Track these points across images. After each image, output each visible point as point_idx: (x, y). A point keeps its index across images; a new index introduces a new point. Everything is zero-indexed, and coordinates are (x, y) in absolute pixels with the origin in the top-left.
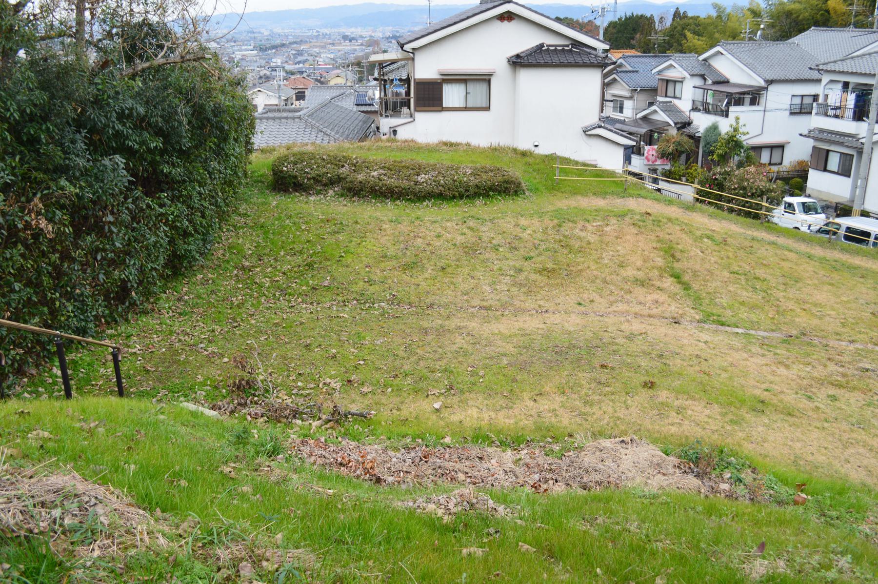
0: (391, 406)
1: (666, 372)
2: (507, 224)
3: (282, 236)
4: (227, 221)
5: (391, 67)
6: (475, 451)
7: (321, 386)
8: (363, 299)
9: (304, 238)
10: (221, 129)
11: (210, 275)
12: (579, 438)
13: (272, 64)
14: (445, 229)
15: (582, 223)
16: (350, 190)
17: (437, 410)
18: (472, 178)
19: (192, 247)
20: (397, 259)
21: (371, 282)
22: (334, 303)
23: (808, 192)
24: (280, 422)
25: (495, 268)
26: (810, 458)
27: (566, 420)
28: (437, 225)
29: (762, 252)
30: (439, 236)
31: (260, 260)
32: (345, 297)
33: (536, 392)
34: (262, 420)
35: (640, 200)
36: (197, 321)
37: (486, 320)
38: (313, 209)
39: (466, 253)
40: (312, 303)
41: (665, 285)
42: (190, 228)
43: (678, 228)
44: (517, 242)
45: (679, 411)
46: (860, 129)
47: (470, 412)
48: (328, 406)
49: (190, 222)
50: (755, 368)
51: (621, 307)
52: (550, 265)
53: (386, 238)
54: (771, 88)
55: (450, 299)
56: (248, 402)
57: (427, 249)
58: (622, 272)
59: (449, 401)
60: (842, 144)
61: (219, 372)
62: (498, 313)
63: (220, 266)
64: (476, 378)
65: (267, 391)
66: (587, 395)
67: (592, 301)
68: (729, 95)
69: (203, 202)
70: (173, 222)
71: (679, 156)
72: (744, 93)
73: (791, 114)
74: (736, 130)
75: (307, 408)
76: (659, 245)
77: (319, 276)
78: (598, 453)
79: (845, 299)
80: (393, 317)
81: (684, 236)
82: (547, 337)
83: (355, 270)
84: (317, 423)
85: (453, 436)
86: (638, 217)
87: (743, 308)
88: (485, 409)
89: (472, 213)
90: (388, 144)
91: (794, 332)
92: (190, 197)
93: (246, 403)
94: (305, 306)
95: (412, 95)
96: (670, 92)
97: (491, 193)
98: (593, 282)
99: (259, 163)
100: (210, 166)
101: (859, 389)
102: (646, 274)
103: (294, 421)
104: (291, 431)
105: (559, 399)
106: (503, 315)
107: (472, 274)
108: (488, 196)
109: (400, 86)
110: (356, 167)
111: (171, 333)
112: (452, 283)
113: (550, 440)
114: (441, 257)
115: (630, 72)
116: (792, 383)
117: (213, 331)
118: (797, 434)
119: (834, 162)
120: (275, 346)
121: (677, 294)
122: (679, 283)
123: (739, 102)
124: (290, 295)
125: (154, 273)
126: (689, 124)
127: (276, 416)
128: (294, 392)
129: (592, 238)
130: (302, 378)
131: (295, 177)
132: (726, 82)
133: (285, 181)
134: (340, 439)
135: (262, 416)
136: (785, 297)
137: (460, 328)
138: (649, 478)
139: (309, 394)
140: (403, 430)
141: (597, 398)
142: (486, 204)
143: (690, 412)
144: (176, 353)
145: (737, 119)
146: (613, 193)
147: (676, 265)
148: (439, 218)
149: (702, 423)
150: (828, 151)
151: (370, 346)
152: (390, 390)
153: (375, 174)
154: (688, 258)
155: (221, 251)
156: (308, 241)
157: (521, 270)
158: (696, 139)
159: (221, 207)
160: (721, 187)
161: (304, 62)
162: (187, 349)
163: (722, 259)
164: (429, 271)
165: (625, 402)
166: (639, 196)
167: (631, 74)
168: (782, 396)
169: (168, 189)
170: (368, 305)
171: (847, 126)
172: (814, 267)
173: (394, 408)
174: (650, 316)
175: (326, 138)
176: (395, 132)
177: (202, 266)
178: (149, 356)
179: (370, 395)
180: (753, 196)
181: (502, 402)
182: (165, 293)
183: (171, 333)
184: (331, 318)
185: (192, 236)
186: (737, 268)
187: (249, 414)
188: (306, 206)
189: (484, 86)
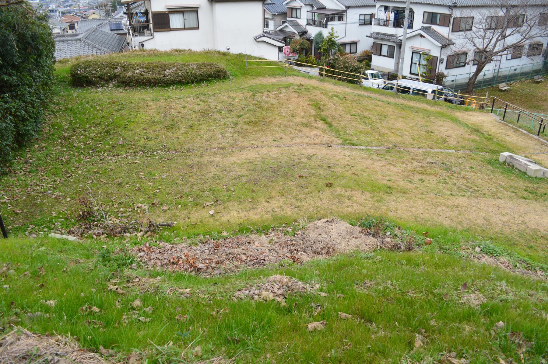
0: (183, 216)
1: (335, 176)
2: (224, 96)
3: (85, 115)
4: (47, 108)
5: (134, 6)
6: (244, 239)
7: (136, 209)
8: (145, 150)
9: (99, 115)
10: (38, 49)
11: (43, 145)
12: (301, 223)
13: (50, 8)
14: (187, 102)
15: (266, 93)
16: (123, 82)
17: (212, 215)
18: (198, 71)
19: (30, 128)
20: (161, 123)
21: (149, 139)
22: (128, 154)
23: (372, 67)
24: (116, 236)
25: (222, 123)
26: (422, 216)
27: (289, 212)
28: (182, 100)
29: (365, 102)
30: (184, 107)
31: (74, 131)
32: (134, 150)
33: (267, 197)
34: (103, 236)
35: (295, 77)
36: (42, 175)
37: (224, 156)
38: (101, 96)
39: (203, 116)
40: (114, 156)
41: (319, 125)
42: (27, 116)
43: (319, 92)
44: (231, 107)
45: (349, 198)
46: (399, 32)
47: (232, 214)
48: (145, 221)
49: (26, 111)
50: (380, 169)
51: (298, 140)
52: (253, 119)
53: (152, 111)
54: (350, 11)
55: (199, 145)
56: (92, 226)
57: (179, 115)
58: (294, 120)
59: (218, 208)
60: (389, 40)
61: (66, 208)
62: (230, 151)
63: (49, 138)
64: (230, 192)
65: (102, 217)
66: (297, 195)
67: (281, 138)
68: (326, 15)
69: (32, 98)
70: (15, 112)
71: (303, 51)
72: (334, 14)
73: (360, 25)
74: (332, 35)
75: (131, 225)
76: (311, 103)
77: (115, 138)
78: (316, 230)
79: (411, 125)
80: (168, 159)
81: (323, 96)
82: (263, 162)
83: (137, 132)
84: (139, 234)
85: (227, 230)
86: (296, 87)
87: (362, 135)
88: (240, 211)
89: (201, 92)
90: (141, 53)
91: (391, 146)
92: (24, 95)
93: (90, 227)
94: (110, 158)
95: (151, 22)
96: (294, 15)
97: (210, 79)
98: (279, 127)
99: (61, 70)
100: (33, 73)
101: (432, 174)
102: (307, 120)
103: (125, 234)
104: (125, 242)
105: (282, 200)
106: (233, 152)
107: (209, 128)
108: (208, 81)
109: (143, 16)
110: (125, 68)
111: (26, 185)
112: (198, 135)
113: (285, 225)
114: (188, 120)
115: (270, 4)
116: (400, 175)
117: (55, 181)
118: (411, 203)
119: (385, 50)
120: (99, 186)
121: (326, 130)
122: (326, 123)
123: (332, 19)
124: (99, 152)
125: (8, 148)
126: (306, 32)
127: (112, 233)
128: (119, 215)
129: (274, 101)
130: (122, 205)
131: (87, 77)
132: (324, 8)
133: (80, 80)
134: (158, 242)
135: (103, 234)
136: (381, 126)
137: (210, 162)
138: (349, 241)
139: (130, 215)
140: (196, 231)
141: (303, 196)
142: (208, 86)
143: (355, 198)
144: (33, 199)
145: (332, 29)
146: (279, 74)
147: (322, 113)
148: (182, 96)
149: (362, 203)
150: (381, 45)
151: (159, 179)
152: (180, 206)
153: (138, 71)
154: (328, 109)
155: (47, 128)
156: (103, 117)
157: (237, 124)
158: (310, 41)
159: (43, 100)
160: (333, 67)
161: (70, 6)
162: (40, 195)
163: (345, 108)
164: (183, 129)
165: (319, 196)
166: (294, 75)
167: (271, 5)
168: (398, 183)
169: (7, 91)
170: (149, 154)
171: (391, 30)
172: (392, 109)
173: (185, 217)
174: (315, 144)
175: (99, 52)
176: (143, 45)
177: (37, 139)
178: (15, 203)
179: (168, 211)
180: (351, 71)
181: (250, 205)
182: (15, 159)
183: (26, 185)
184: (130, 164)
185: (28, 120)
186: (354, 113)
187: (94, 234)
188: (97, 95)
189: (194, 15)
